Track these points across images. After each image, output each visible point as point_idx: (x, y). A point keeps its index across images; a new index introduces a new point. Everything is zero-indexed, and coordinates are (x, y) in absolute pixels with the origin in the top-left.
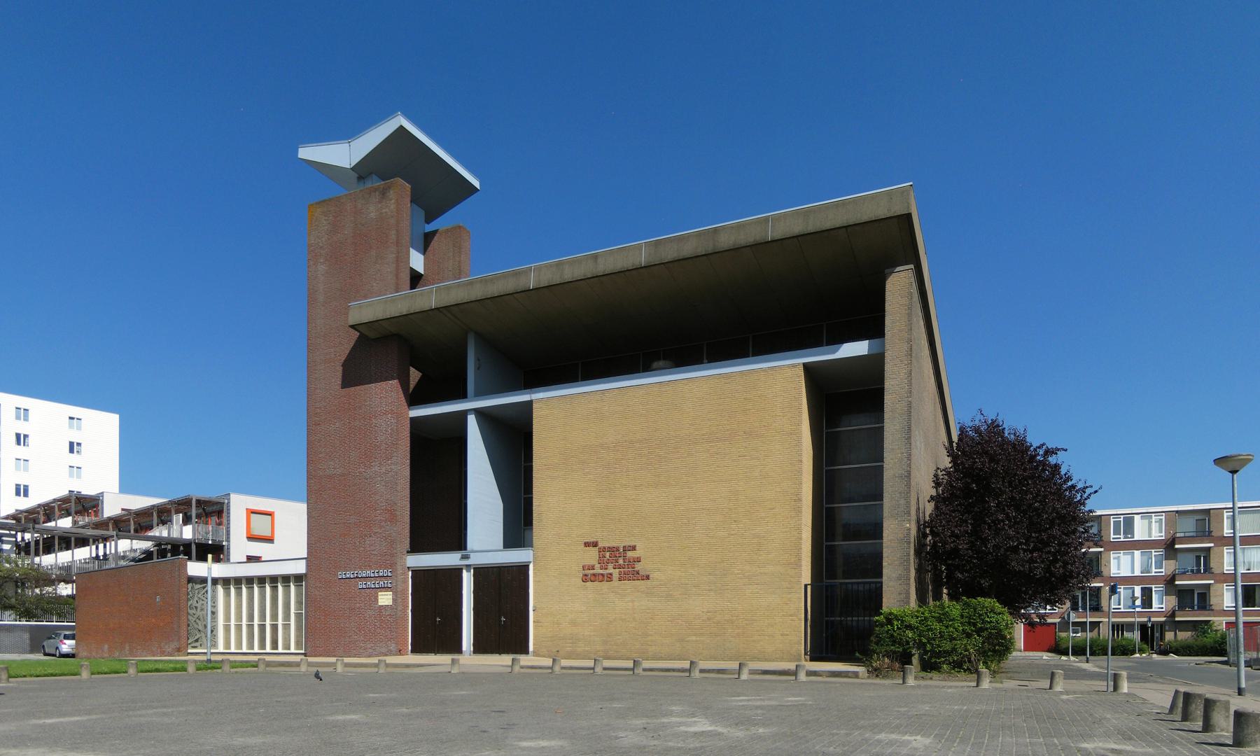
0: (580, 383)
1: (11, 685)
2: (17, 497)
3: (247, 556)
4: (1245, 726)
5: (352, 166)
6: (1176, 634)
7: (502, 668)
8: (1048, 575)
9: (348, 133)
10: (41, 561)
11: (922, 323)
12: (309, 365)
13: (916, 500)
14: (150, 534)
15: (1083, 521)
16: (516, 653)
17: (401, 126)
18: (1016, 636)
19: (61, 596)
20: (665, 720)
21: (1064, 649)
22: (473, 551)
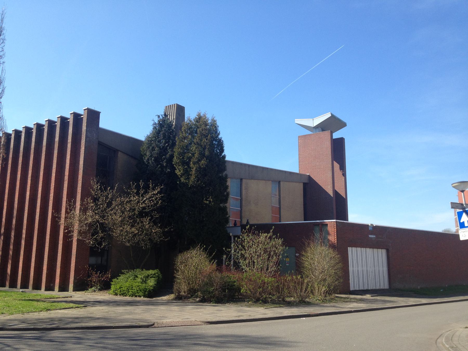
0: (211, 304)
1: (30, 315)
2: (97, 109)
3: (451, 203)
4: (235, 303)
5: (314, 126)
6: (239, 226)
7: (341, 306)
8: (102, 166)
9: (313, 117)
10: (238, 226)
11: (278, 192)
12: (300, 156)
13: (63, 298)
14: (10, 273)
15: (304, 267)
16: (15, 229)
17: (54, 291)
18: (360, 298)
19: (226, 181)
20: (82, 341)
21: (455, 232)
22: (228, 178)
